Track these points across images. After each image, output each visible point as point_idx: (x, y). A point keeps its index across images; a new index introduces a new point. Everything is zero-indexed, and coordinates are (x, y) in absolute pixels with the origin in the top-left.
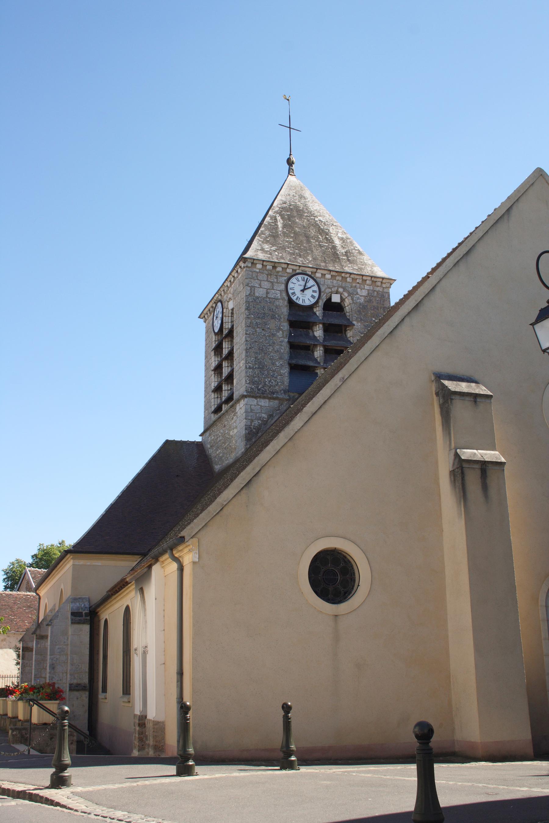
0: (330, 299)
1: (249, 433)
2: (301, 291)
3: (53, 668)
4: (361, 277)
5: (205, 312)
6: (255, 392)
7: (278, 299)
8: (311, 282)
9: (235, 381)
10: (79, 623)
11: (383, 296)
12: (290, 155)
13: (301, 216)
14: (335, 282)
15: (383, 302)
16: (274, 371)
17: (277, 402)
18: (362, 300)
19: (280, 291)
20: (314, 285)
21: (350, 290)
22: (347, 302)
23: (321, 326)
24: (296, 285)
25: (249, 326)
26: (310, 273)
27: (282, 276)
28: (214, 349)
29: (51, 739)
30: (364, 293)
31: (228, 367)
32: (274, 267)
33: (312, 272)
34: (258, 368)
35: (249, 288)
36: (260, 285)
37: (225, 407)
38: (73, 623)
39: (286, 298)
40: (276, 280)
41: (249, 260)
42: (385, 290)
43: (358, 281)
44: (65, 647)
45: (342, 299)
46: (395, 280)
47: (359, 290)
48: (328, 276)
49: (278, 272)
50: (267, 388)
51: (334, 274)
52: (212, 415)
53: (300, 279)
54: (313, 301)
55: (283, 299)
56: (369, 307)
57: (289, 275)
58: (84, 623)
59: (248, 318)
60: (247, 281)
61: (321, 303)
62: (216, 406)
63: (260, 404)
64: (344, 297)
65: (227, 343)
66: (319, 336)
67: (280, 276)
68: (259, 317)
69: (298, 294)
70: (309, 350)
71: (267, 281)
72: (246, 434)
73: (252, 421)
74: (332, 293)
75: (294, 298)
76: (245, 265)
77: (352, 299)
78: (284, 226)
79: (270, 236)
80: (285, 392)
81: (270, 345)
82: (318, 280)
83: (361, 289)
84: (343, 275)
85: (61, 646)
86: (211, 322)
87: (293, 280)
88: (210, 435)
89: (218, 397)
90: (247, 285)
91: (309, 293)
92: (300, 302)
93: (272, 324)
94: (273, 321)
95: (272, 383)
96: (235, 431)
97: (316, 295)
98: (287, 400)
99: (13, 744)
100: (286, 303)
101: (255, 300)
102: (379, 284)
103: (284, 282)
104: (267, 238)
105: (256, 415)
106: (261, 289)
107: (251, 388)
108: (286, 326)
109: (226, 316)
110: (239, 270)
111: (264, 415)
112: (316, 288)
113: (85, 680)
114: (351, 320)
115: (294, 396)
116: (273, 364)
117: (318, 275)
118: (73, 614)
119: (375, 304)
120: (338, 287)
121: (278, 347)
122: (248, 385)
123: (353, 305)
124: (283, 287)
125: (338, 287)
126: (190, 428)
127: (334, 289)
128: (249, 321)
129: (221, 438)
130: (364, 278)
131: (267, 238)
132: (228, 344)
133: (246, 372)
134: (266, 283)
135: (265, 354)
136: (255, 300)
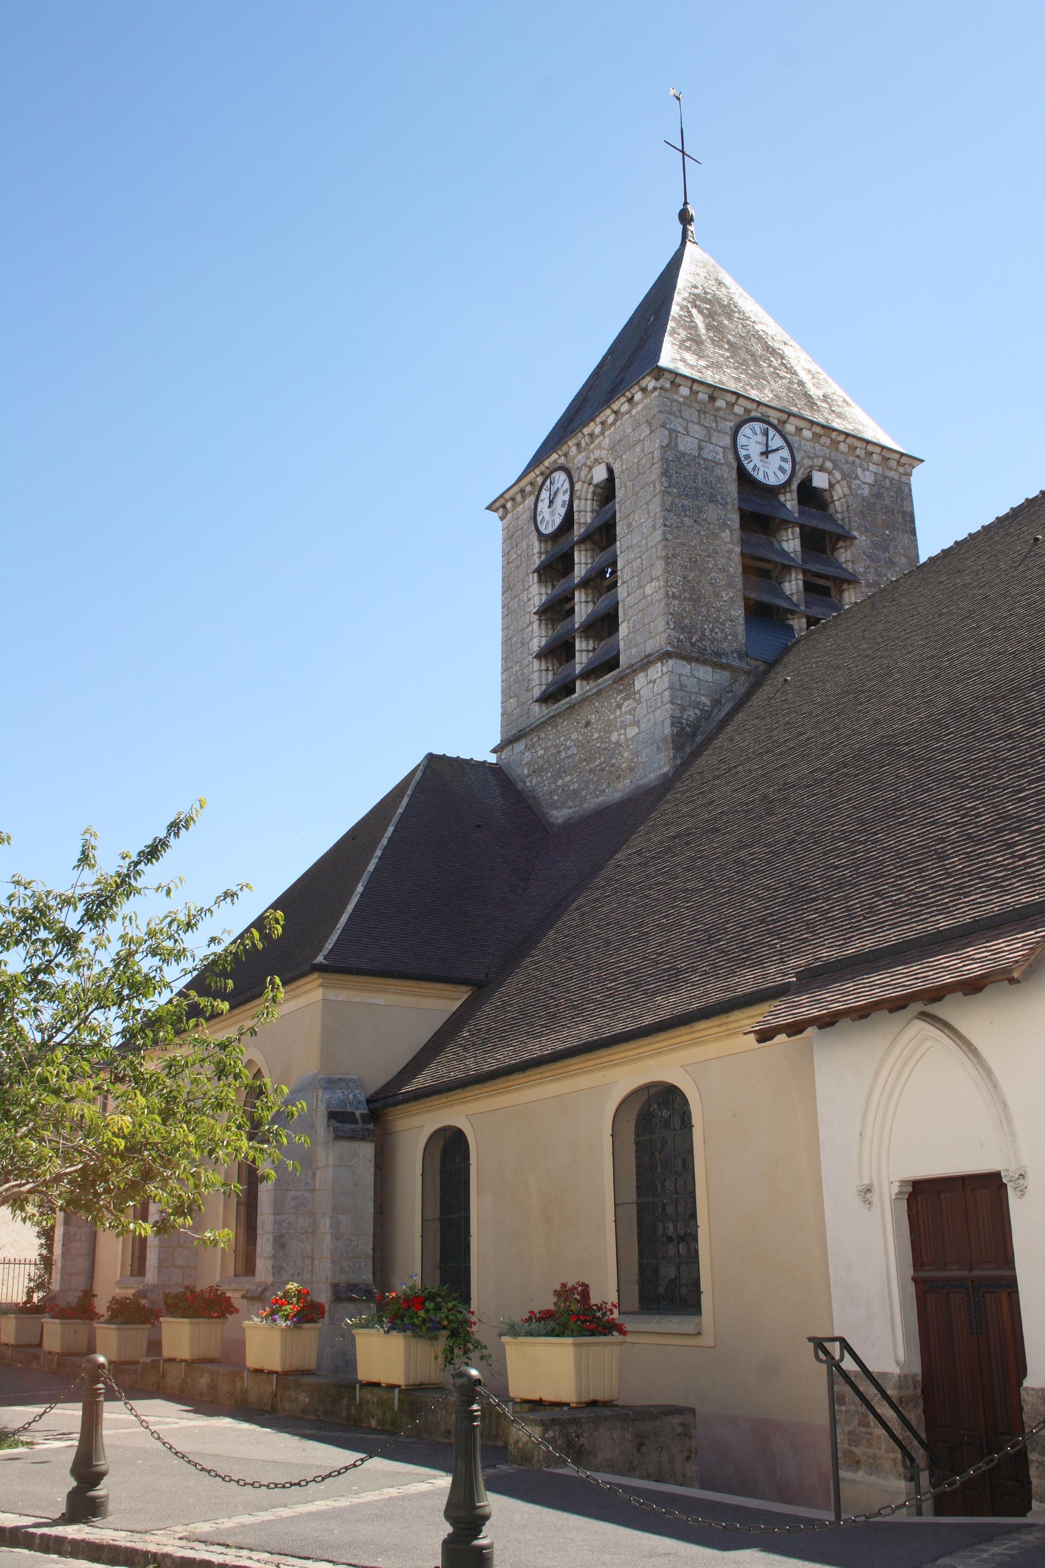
0: (809, 479)
1: (678, 735)
2: (762, 454)
3: (283, 1246)
4: (864, 445)
5: (507, 496)
6: (686, 649)
7: (721, 464)
8: (776, 442)
9: (623, 630)
10: (353, 1137)
11: (900, 490)
12: (686, 203)
13: (730, 317)
14: (818, 447)
15: (902, 500)
16: (719, 610)
17: (726, 674)
18: (866, 491)
19: (722, 447)
20: (782, 448)
21: (845, 467)
22: (838, 492)
23: (797, 530)
24: (751, 440)
25: (670, 511)
26: (775, 422)
27: (725, 419)
28: (537, 571)
29: (639, 1447)
30: (869, 478)
31: (587, 602)
32: (712, 399)
33: (779, 420)
34: (690, 600)
35: (667, 433)
36: (686, 429)
37: (582, 686)
38: (339, 1137)
39: (735, 465)
40: (714, 425)
41: (666, 375)
42: (904, 479)
43: (858, 452)
44: (307, 1195)
45: (831, 486)
46: (922, 461)
47: (859, 471)
48: (807, 434)
49: (718, 409)
50: (707, 643)
51: (817, 430)
52: (536, 708)
53: (758, 431)
54: (783, 478)
55: (729, 465)
56: (878, 507)
57: (738, 420)
58: (363, 1139)
59: (668, 492)
60: (663, 417)
61: (794, 486)
62: (544, 687)
63: (697, 675)
64: (834, 482)
65: (583, 553)
66: (795, 551)
67: (722, 418)
68: (687, 495)
69: (756, 459)
70: (770, 578)
71: (699, 423)
72: (673, 736)
73: (683, 709)
74: (812, 468)
75: (749, 467)
76: (658, 384)
77: (849, 487)
78: (709, 327)
79: (688, 339)
80: (743, 655)
81: (709, 556)
82: (789, 437)
83: (864, 470)
84: (834, 435)
85: (299, 1194)
86: (527, 515)
87: (746, 429)
88: (527, 748)
89: (547, 670)
90: (663, 425)
91: (774, 459)
92: (760, 477)
93: (712, 513)
94: (712, 506)
95: (716, 633)
96: (632, 732)
97: (788, 467)
98: (745, 673)
99: (548, 1467)
100: (734, 474)
101: (679, 460)
102: (893, 464)
103: (728, 430)
104: (684, 341)
105: (690, 697)
106: (689, 439)
107: (679, 640)
108: (735, 519)
109: (580, 499)
110: (638, 396)
111: (704, 699)
112: (785, 453)
113: (367, 1276)
114: (847, 527)
115: (757, 667)
116: (717, 595)
117: (790, 428)
118: (333, 1116)
119: (887, 502)
120: (825, 458)
121: (723, 561)
122: (672, 633)
123: (850, 499)
124: (727, 441)
125: (825, 458)
126: (474, 734)
127: (818, 462)
128: (670, 499)
129: (574, 750)
130: (870, 448)
131: (684, 341)
132: (586, 556)
133: (668, 605)
134: (697, 427)
135: (702, 571)
136: (679, 460)
